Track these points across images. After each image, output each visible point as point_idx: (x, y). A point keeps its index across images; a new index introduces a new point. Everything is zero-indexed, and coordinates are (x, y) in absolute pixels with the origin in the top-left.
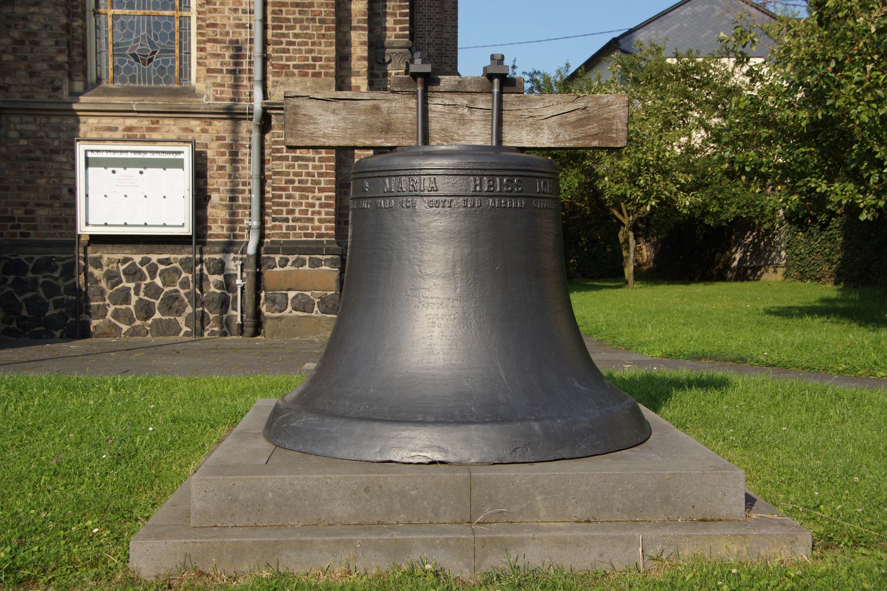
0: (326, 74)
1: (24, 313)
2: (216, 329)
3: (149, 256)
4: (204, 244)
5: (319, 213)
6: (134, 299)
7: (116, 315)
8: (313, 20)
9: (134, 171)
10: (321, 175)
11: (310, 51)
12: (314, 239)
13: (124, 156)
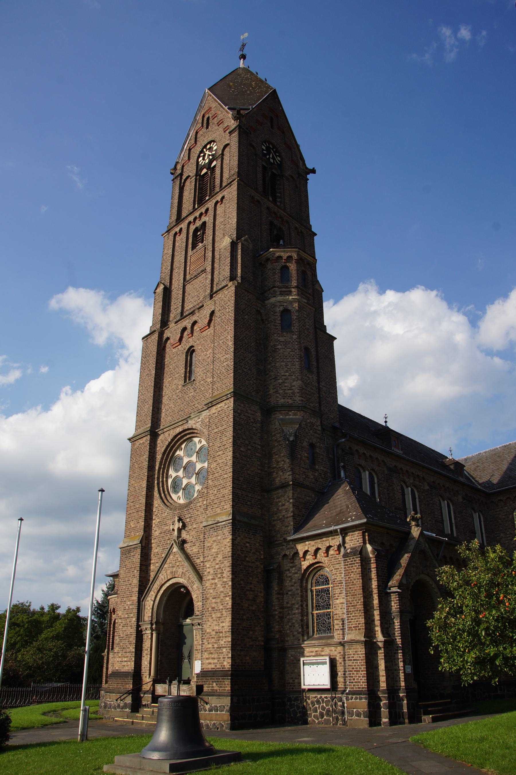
0: (362, 629)
1: (292, 715)
2: (341, 723)
3: (322, 695)
4: (337, 691)
5: (362, 679)
6: (318, 711)
8: (357, 610)
9: (315, 666)
10: (361, 665)
11: (357, 621)
12: (361, 689)
13: (313, 661)
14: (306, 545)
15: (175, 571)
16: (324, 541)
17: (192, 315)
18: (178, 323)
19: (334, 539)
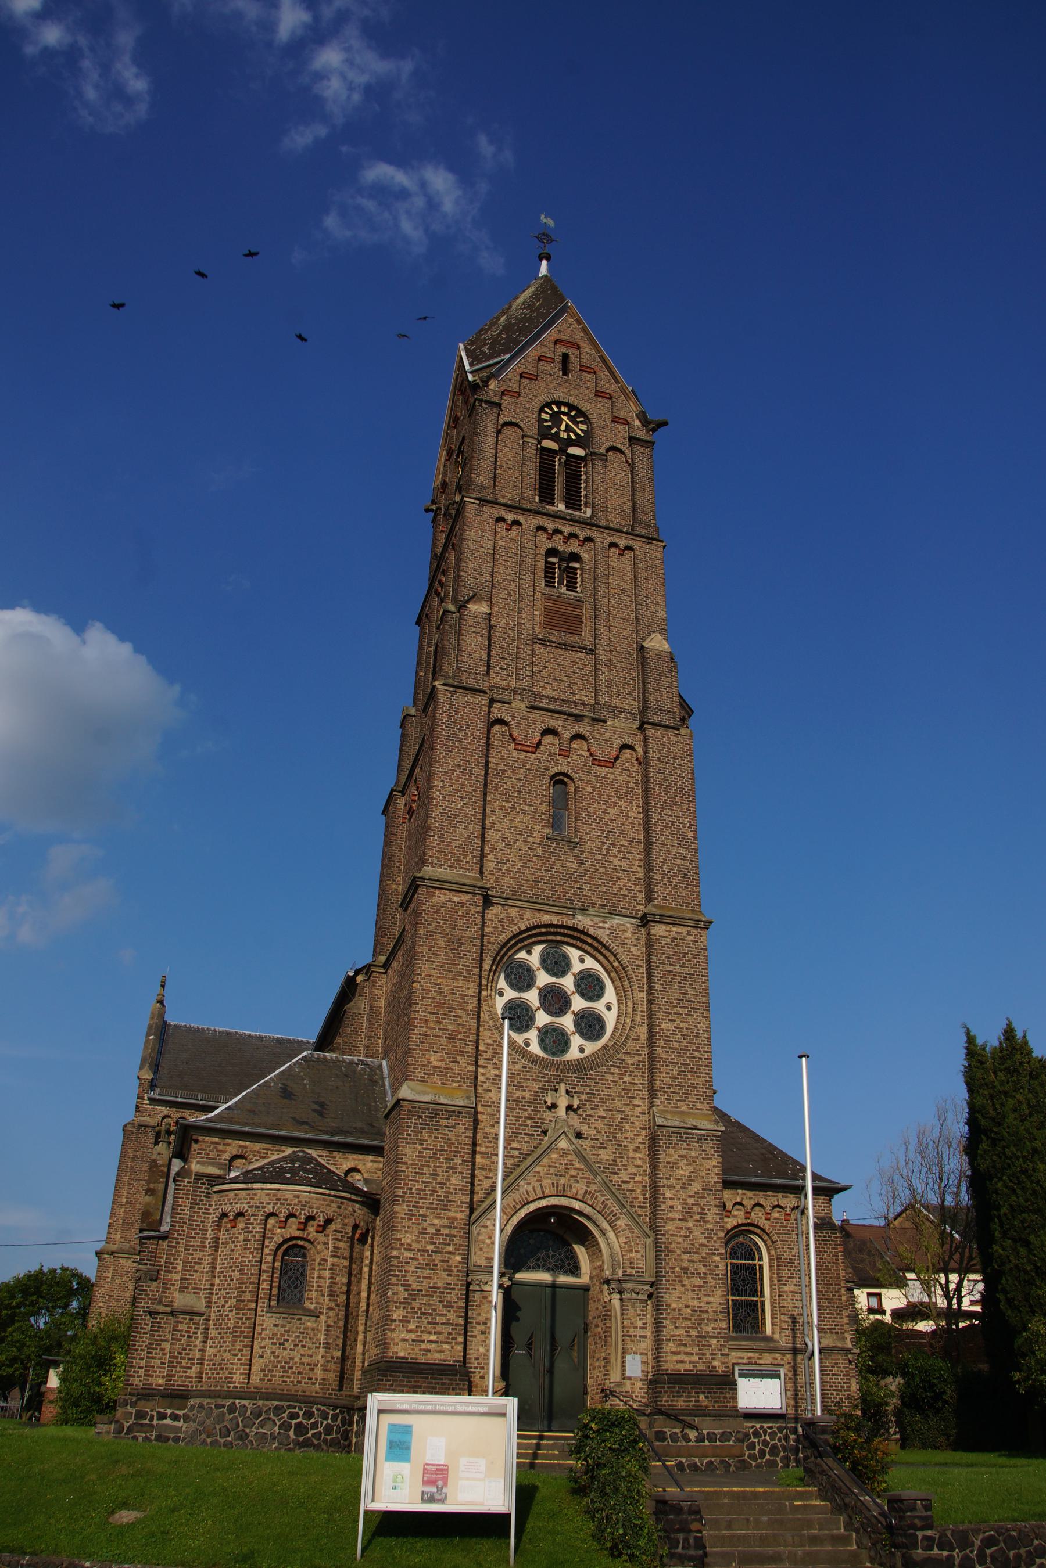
6: (757, 1447)
7: (750, 1456)
11: (833, 1321)
14: (738, 1194)
15: (564, 1185)
16: (769, 1196)
17: (574, 718)
18: (536, 711)
19: (787, 1197)
